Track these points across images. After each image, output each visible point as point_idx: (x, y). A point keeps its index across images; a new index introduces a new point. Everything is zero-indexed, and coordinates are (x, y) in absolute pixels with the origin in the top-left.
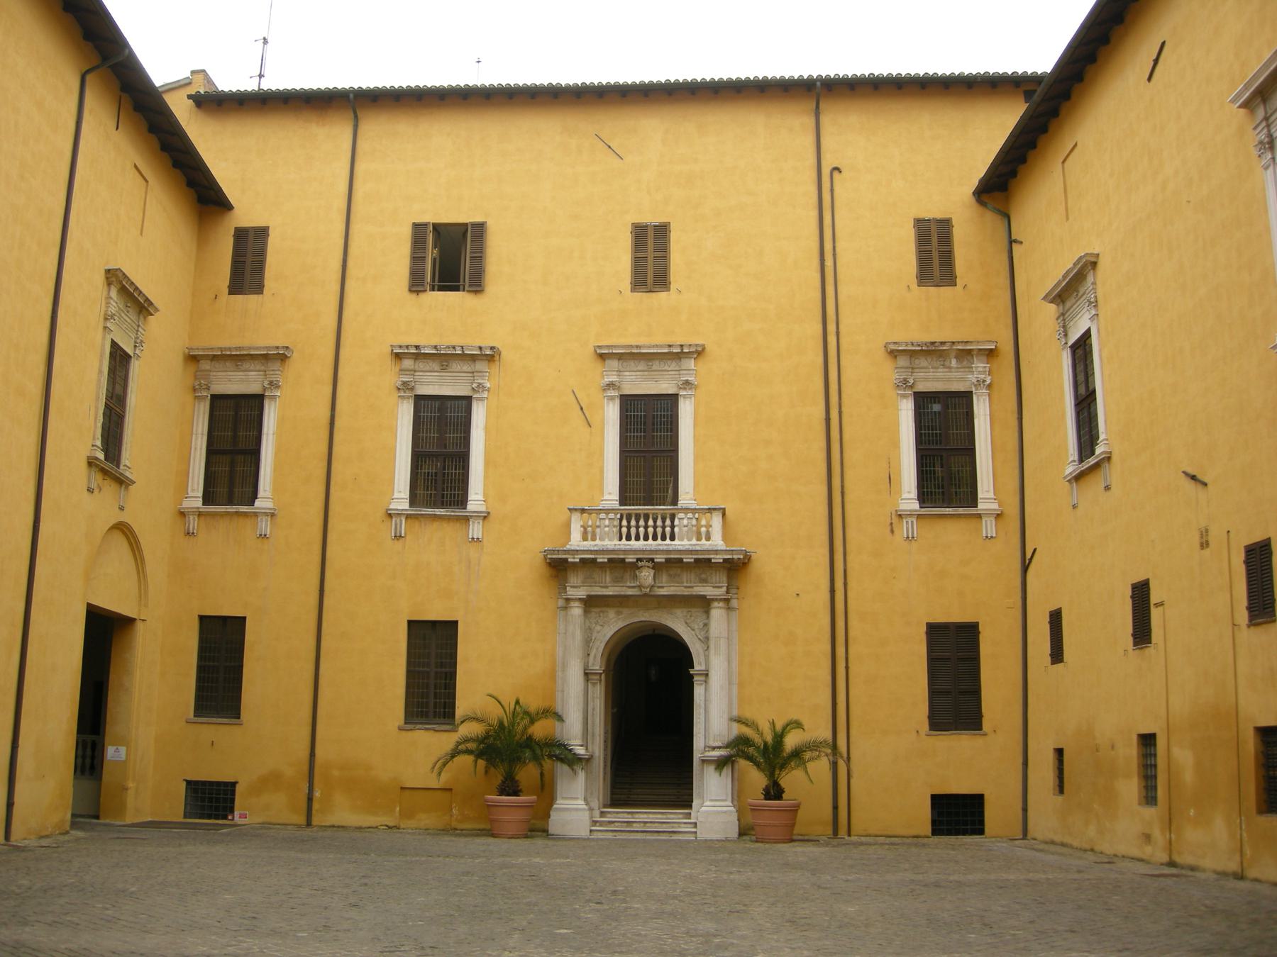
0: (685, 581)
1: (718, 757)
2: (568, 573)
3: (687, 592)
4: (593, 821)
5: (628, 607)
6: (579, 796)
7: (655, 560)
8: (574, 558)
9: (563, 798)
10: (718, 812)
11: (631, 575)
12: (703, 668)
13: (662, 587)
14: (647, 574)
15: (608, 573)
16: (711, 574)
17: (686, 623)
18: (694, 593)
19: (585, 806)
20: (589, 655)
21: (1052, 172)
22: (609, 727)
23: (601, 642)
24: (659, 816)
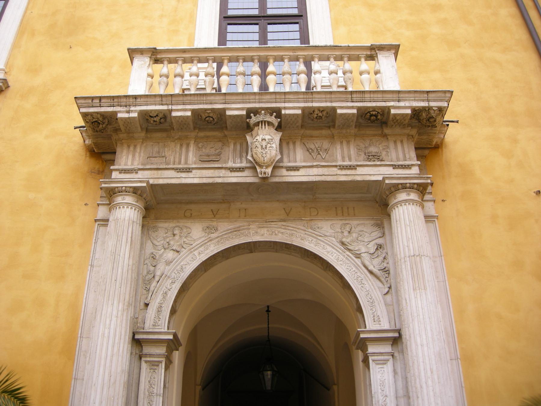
0: (339, 157)
2: (118, 150)
3: (343, 176)
5: (227, 217)
7: (283, 112)
8: (128, 112)
11: (235, 150)
13: (297, 169)
14: (267, 137)
15: (192, 148)
16: (388, 147)
17: (343, 243)
18: (359, 178)
20: (147, 305)
21: (379, 347)
23: (173, 283)
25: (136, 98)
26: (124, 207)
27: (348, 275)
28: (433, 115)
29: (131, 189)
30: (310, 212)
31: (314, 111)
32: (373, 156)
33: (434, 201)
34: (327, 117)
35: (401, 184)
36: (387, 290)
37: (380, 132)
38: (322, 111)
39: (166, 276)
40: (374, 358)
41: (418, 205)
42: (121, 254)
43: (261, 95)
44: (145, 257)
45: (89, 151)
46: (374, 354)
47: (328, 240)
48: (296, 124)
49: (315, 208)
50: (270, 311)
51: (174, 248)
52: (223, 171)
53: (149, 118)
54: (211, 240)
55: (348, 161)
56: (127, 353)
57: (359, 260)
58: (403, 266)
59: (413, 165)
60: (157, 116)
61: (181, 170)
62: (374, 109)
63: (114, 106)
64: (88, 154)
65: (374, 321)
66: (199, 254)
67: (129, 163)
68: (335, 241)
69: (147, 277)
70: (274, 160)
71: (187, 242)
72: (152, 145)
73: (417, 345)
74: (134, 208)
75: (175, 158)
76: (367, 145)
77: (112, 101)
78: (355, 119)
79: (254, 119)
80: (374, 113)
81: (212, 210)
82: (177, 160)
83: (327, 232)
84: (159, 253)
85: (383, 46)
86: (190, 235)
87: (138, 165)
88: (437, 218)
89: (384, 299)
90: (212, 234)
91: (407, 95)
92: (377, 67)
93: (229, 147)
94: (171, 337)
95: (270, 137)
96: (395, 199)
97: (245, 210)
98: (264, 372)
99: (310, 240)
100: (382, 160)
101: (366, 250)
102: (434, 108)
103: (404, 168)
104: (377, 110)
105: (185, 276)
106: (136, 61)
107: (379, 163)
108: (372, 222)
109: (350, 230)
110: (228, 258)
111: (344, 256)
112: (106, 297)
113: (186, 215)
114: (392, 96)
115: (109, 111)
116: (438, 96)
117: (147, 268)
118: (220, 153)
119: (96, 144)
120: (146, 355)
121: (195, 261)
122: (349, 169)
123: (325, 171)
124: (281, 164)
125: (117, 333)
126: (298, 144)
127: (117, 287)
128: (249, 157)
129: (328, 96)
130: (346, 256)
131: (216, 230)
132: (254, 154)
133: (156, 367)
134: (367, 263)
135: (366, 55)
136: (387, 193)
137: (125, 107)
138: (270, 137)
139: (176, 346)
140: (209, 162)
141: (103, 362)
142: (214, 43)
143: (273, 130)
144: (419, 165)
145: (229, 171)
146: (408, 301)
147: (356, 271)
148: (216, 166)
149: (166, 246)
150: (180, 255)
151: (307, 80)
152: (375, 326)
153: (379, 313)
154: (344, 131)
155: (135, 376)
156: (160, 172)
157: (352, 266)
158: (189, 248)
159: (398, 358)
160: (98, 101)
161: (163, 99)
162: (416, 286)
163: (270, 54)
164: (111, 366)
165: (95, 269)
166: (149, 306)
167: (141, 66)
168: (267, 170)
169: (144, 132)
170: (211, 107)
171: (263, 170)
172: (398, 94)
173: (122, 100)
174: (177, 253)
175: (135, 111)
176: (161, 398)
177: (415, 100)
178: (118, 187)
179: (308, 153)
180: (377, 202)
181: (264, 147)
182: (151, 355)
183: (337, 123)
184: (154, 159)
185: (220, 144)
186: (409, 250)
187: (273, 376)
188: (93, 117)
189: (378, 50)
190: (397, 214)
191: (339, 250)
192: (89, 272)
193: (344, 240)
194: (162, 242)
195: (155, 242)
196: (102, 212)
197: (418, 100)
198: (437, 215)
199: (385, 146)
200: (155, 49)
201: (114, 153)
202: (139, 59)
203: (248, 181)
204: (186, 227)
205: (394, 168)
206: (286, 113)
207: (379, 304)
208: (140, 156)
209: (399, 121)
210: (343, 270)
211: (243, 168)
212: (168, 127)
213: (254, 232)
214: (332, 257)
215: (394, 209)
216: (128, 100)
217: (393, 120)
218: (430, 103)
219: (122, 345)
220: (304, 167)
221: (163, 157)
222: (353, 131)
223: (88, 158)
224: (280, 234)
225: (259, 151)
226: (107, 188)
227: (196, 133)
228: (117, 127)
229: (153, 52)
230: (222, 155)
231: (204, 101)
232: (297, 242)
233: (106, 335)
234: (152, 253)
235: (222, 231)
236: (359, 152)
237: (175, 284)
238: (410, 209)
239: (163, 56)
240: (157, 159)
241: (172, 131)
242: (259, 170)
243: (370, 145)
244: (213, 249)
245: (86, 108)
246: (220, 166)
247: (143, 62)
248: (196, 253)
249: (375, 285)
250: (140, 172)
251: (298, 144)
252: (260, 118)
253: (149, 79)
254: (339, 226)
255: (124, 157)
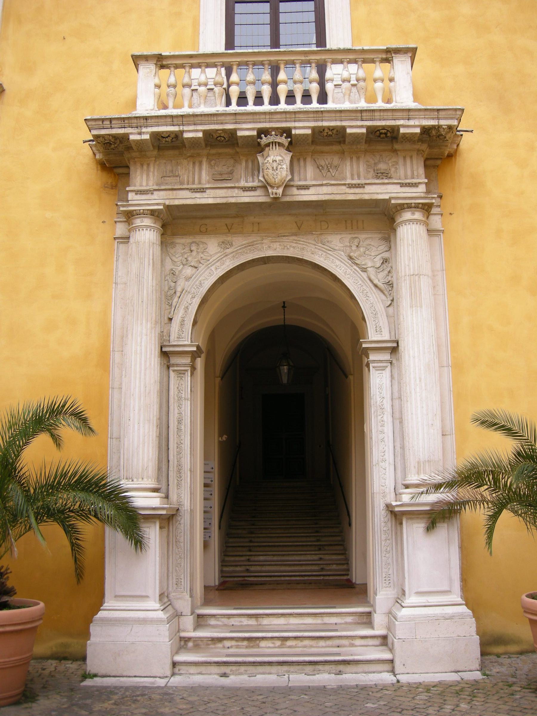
0: (348, 175)
1: (433, 504)
2: (132, 168)
3: (351, 195)
4: (181, 638)
5: (241, 233)
6: (150, 593)
7: (293, 132)
8: (140, 134)
9: (117, 597)
10: (436, 619)
11: (247, 167)
12: (386, 336)
13: (307, 187)
14: (278, 158)
15: (205, 166)
16: (397, 163)
17: (351, 258)
18: (366, 197)
19: (161, 615)
20: (170, 319)
22: (215, 464)
23: (193, 297)
24: (309, 620)
25: (146, 119)
26: (143, 230)
27: (355, 288)
28: (442, 133)
29: (148, 211)
30: (321, 225)
31: (324, 130)
32: (382, 173)
33: (442, 215)
34: (337, 134)
35: (407, 204)
36: (389, 302)
37: (390, 148)
38: (332, 130)
39: (187, 291)
40: (373, 365)
41: (422, 224)
42: (145, 277)
43: (271, 115)
44: (166, 274)
45: (100, 164)
46: (374, 361)
47: (337, 254)
48: (306, 142)
49: (326, 221)
50: (286, 307)
51: (192, 264)
52: (236, 191)
53: (161, 138)
54: (226, 256)
55: (357, 179)
56: (158, 365)
57: (365, 273)
58: (403, 285)
59: (420, 183)
60: (169, 136)
61: (196, 190)
62: (383, 128)
63: (125, 128)
64: (99, 167)
65: (376, 332)
66: (216, 269)
67: (144, 183)
68: (344, 255)
69: (169, 293)
70: (285, 181)
71: (204, 257)
72: (165, 163)
73: (409, 357)
74: (152, 230)
75: (188, 177)
76: (376, 161)
77: (123, 122)
78: (365, 137)
79: (264, 140)
80: (383, 131)
81: (226, 225)
82: (191, 180)
83: (337, 246)
84: (178, 269)
85: (400, 49)
86: (207, 250)
87: (153, 185)
88: (443, 232)
89: (386, 311)
90: (228, 250)
91: (417, 113)
92: (392, 75)
93: (241, 164)
94: (195, 349)
95: (280, 158)
96: (401, 217)
97: (259, 223)
98: (281, 367)
99: (320, 254)
100: (390, 178)
101: (372, 265)
102: (443, 127)
103: (411, 186)
104: (386, 129)
105: (204, 290)
106: (141, 68)
107: (386, 181)
108: (380, 236)
109: (359, 244)
110: (243, 270)
111: (351, 270)
112: (135, 317)
113: (201, 230)
114: (401, 115)
115: (121, 134)
116: (449, 113)
117: (168, 284)
118: (232, 171)
119: (108, 161)
120: (173, 365)
121: (212, 276)
122: (357, 187)
123: (334, 189)
124: (292, 183)
125: (148, 349)
126: (309, 160)
127: (144, 307)
128: (261, 178)
129: (338, 115)
130: (353, 270)
131: (231, 245)
132: (265, 175)
133: (182, 375)
134: (373, 277)
135: (381, 58)
136: (394, 210)
137: (136, 128)
138: (280, 158)
139: (198, 354)
140: (222, 181)
141: (138, 375)
142: (220, 48)
143: (283, 151)
144: (426, 184)
145: (242, 190)
146: (405, 317)
147: (362, 284)
148: (229, 185)
149: (184, 262)
150: (199, 271)
151: (319, 88)
152: (376, 336)
153: (381, 324)
154: (355, 147)
155: (165, 384)
156: (175, 192)
157: (359, 280)
158: (206, 263)
159: (396, 364)
160: (109, 123)
161: (174, 119)
162: (413, 304)
163: (280, 59)
164: (145, 379)
165: (119, 286)
166: (173, 320)
167: (147, 75)
168: (278, 191)
169: (157, 151)
170: (222, 128)
171: (274, 191)
172: (408, 113)
173: (133, 121)
174: (195, 269)
175: (147, 133)
176: (189, 402)
177: (425, 118)
178: (135, 210)
179: (318, 170)
180: (386, 215)
181: (275, 168)
182: (177, 365)
183: (347, 140)
184: (168, 178)
185: (232, 161)
186: (409, 269)
187: (289, 370)
188: (105, 139)
189: (395, 53)
190: (401, 232)
191: (346, 264)
192: (114, 290)
193: (352, 254)
194: (181, 258)
195: (174, 258)
196: (121, 229)
197: (428, 118)
198: (443, 229)
199: (394, 162)
200: (161, 55)
201: (128, 167)
202: (144, 66)
203: (260, 201)
204: (202, 242)
205: (401, 186)
206: (296, 133)
207: (381, 316)
208: (154, 176)
209: (408, 138)
210: (350, 283)
211: (255, 188)
212: (181, 145)
213: (267, 246)
214: (340, 271)
215: (399, 227)
216: (139, 121)
217: (403, 138)
218: (440, 121)
219: (153, 360)
220: (314, 185)
221: (177, 176)
222: (363, 146)
223: (99, 172)
224: (292, 249)
225: (270, 172)
226: (125, 211)
227: (208, 151)
228: (129, 146)
229: (158, 58)
230: (234, 174)
231: (215, 122)
232: (308, 257)
233: (138, 352)
234: (172, 270)
235: (236, 246)
236: (369, 168)
237: (195, 299)
238: (414, 229)
239: (169, 62)
240: (171, 178)
241: (184, 149)
242: (270, 191)
243: (380, 161)
244: (229, 264)
245: (97, 130)
246: (233, 185)
247: (148, 70)
248: (213, 268)
249: (379, 298)
250: (155, 193)
251: (309, 160)
252: (270, 139)
253: (157, 90)
254: (348, 240)
255: (139, 177)
